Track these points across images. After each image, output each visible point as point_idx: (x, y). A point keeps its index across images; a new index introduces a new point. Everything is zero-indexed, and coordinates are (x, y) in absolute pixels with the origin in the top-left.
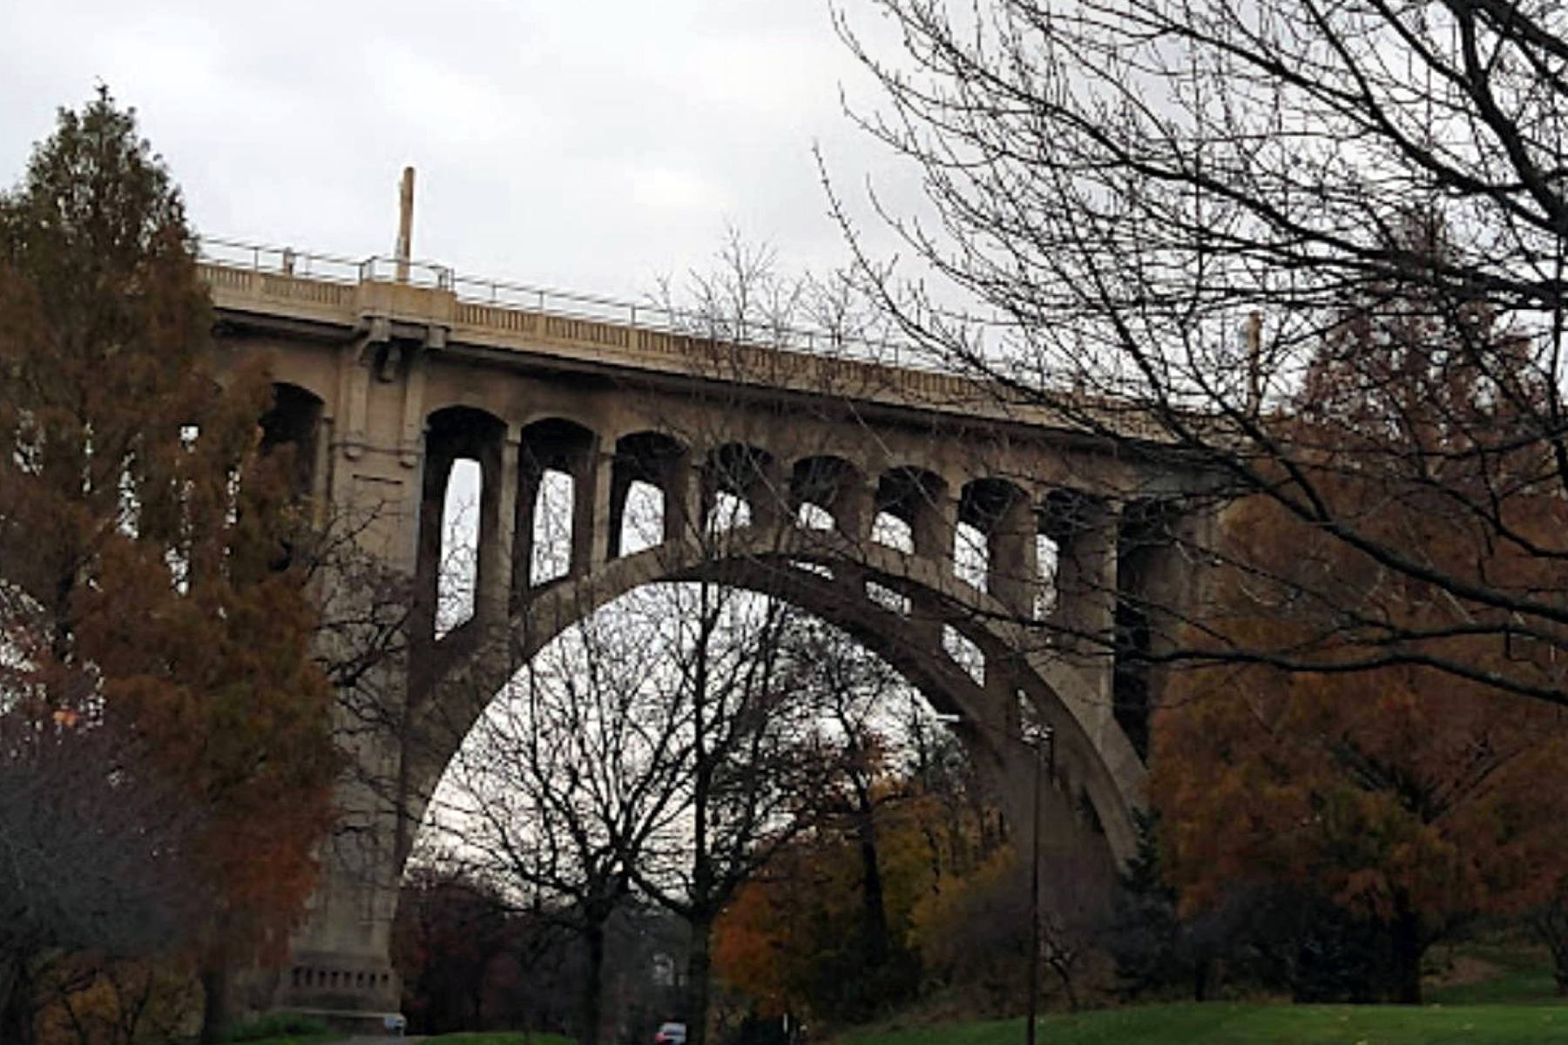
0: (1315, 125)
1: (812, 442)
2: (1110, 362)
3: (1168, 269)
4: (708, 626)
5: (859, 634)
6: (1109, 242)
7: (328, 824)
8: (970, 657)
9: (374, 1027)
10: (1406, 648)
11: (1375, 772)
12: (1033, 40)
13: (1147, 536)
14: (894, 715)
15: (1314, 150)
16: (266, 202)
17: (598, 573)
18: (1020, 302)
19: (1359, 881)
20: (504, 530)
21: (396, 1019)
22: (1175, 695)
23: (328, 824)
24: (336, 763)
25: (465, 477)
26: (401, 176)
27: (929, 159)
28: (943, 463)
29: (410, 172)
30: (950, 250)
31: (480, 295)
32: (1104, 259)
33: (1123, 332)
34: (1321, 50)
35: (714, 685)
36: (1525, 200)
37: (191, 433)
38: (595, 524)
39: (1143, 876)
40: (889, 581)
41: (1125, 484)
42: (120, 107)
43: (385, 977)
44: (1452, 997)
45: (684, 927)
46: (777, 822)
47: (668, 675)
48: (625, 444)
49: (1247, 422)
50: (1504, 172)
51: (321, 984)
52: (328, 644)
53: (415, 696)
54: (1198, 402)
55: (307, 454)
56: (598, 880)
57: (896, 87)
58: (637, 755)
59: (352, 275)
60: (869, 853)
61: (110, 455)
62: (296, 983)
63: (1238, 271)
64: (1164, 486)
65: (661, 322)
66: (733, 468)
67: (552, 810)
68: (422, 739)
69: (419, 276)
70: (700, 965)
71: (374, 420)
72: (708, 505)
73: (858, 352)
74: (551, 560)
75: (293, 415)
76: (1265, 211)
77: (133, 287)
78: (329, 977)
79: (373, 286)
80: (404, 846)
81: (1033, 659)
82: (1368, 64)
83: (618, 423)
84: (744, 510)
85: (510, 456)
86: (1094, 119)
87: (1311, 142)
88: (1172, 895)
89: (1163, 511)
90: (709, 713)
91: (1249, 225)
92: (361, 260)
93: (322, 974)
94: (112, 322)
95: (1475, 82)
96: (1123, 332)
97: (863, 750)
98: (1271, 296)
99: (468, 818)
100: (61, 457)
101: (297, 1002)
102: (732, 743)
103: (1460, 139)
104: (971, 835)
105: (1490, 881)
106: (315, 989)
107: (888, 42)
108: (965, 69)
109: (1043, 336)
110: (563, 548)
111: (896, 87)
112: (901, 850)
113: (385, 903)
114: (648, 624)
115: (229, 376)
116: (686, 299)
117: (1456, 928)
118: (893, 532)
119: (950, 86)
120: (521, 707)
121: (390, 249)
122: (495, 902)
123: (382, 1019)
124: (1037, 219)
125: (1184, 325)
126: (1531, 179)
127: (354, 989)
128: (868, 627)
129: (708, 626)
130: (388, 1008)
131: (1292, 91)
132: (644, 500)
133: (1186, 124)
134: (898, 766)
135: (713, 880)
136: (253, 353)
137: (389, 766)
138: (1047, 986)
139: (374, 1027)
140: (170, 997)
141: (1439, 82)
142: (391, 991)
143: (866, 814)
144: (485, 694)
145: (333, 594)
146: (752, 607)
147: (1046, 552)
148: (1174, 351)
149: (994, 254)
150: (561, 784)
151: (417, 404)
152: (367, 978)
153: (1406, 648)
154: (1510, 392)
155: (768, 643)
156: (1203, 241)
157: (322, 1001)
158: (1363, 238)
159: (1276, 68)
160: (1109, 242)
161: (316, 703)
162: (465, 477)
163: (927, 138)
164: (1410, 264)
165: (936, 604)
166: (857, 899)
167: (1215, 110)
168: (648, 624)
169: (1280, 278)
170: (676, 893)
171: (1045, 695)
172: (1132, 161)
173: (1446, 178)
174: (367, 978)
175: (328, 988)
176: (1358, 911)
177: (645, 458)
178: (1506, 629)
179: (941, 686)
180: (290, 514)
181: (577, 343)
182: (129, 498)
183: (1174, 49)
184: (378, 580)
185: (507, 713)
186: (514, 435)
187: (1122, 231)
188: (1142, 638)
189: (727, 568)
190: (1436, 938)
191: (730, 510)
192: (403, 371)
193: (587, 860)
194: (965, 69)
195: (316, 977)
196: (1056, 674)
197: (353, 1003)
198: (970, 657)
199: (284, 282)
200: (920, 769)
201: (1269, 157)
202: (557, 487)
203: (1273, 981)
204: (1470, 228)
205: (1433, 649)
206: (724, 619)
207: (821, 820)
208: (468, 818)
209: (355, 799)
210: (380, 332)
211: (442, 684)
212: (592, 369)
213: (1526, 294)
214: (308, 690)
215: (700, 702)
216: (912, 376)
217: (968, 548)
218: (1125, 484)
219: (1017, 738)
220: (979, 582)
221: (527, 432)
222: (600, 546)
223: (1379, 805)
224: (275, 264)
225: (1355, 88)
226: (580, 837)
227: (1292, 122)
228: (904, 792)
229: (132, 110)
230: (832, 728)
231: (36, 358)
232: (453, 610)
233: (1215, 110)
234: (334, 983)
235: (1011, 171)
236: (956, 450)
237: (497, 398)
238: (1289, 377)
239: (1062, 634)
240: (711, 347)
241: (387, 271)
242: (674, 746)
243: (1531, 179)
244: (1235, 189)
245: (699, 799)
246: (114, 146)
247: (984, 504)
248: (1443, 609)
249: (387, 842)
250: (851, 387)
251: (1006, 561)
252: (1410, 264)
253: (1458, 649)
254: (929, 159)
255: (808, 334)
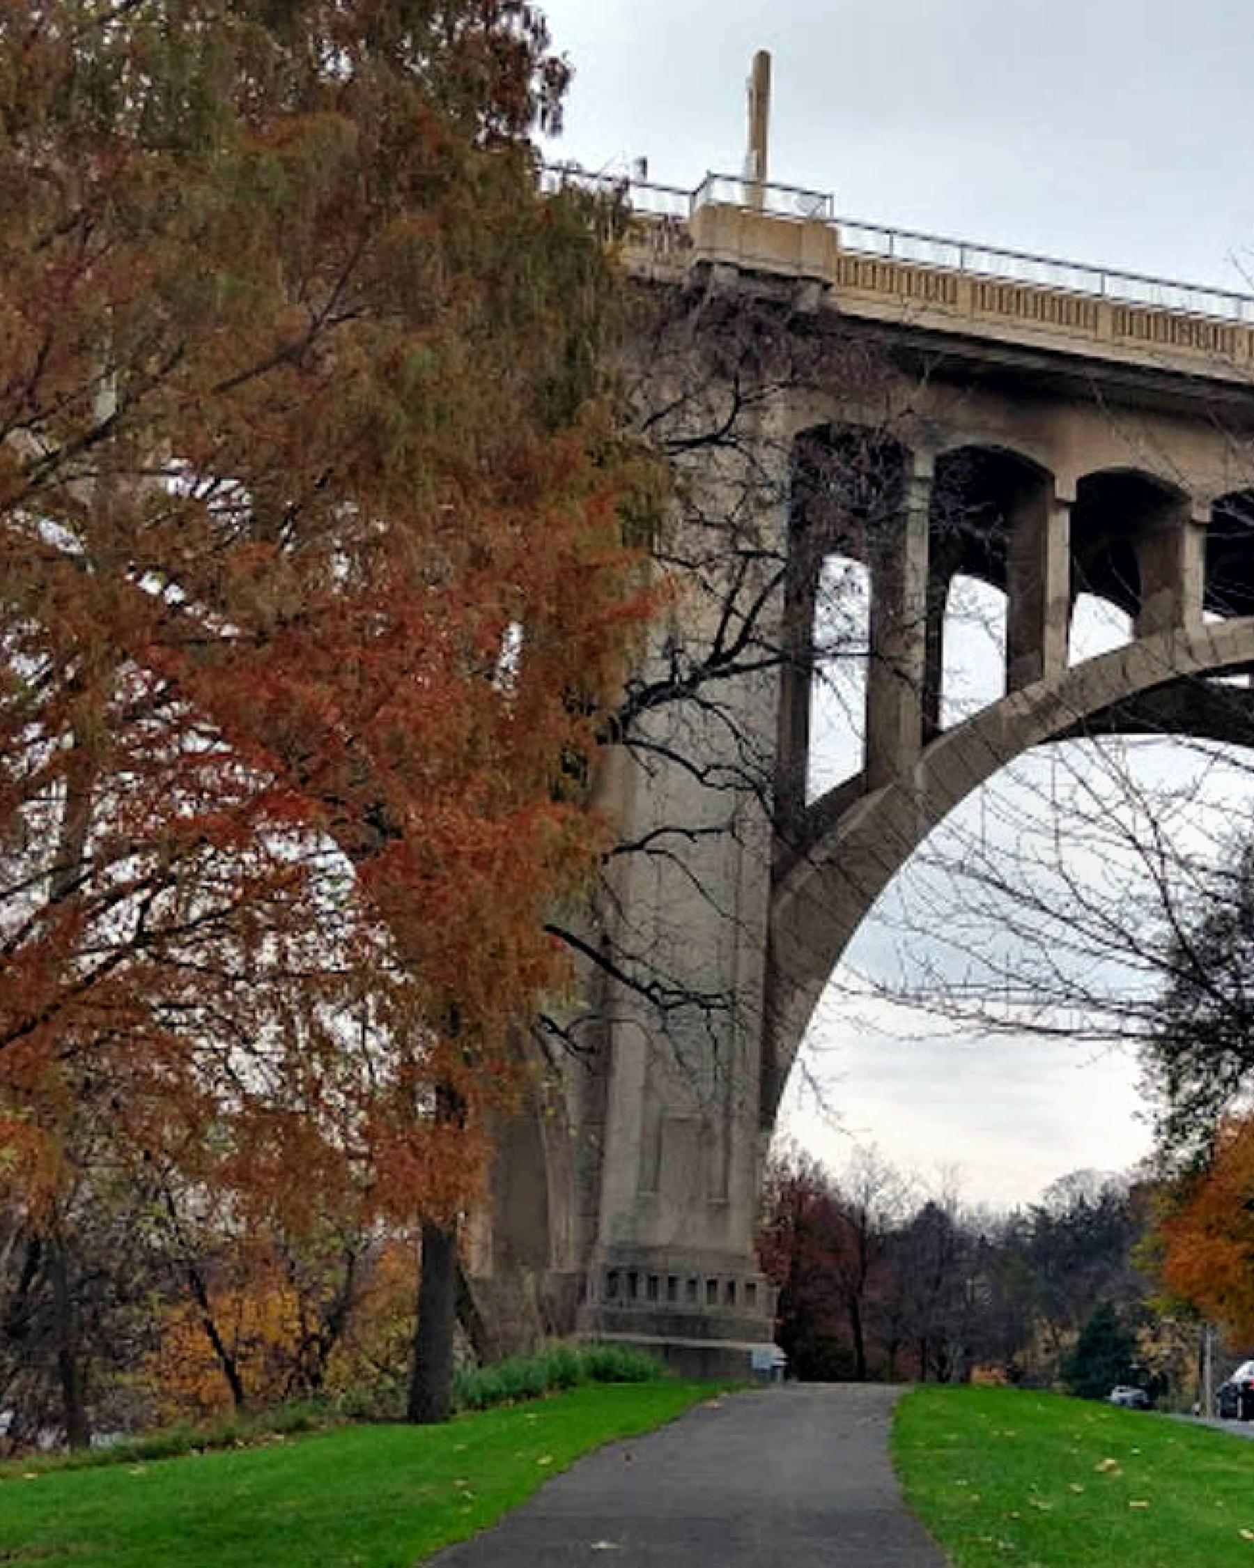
21: (770, 1354)
26: (748, 68)
29: (763, 60)
31: (872, 244)
43: (751, 1287)
51: (653, 1293)
62: (612, 1294)
78: (663, 1285)
79: (715, 213)
92: (692, 187)
93: (653, 1280)
101: (613, 1323)
106: (644, 1304)
121: (735, 160)
123: (750, 1353)
127: (702, 1305)
130: (752, 1334)
142: (761, 1310)
144: (904, 849)
152: (721, 1287)
157: (659, 1322)
161: (294, 775)
174: (721, 1287)
175: (662, 1301)
181: (1022, 321)
186: (923, 467)
195: (642, 1287)
197: (701, 1325)
212: (1039, 363)
221: (941, 464)
229: (874, 1145)
234: (672, 1296)
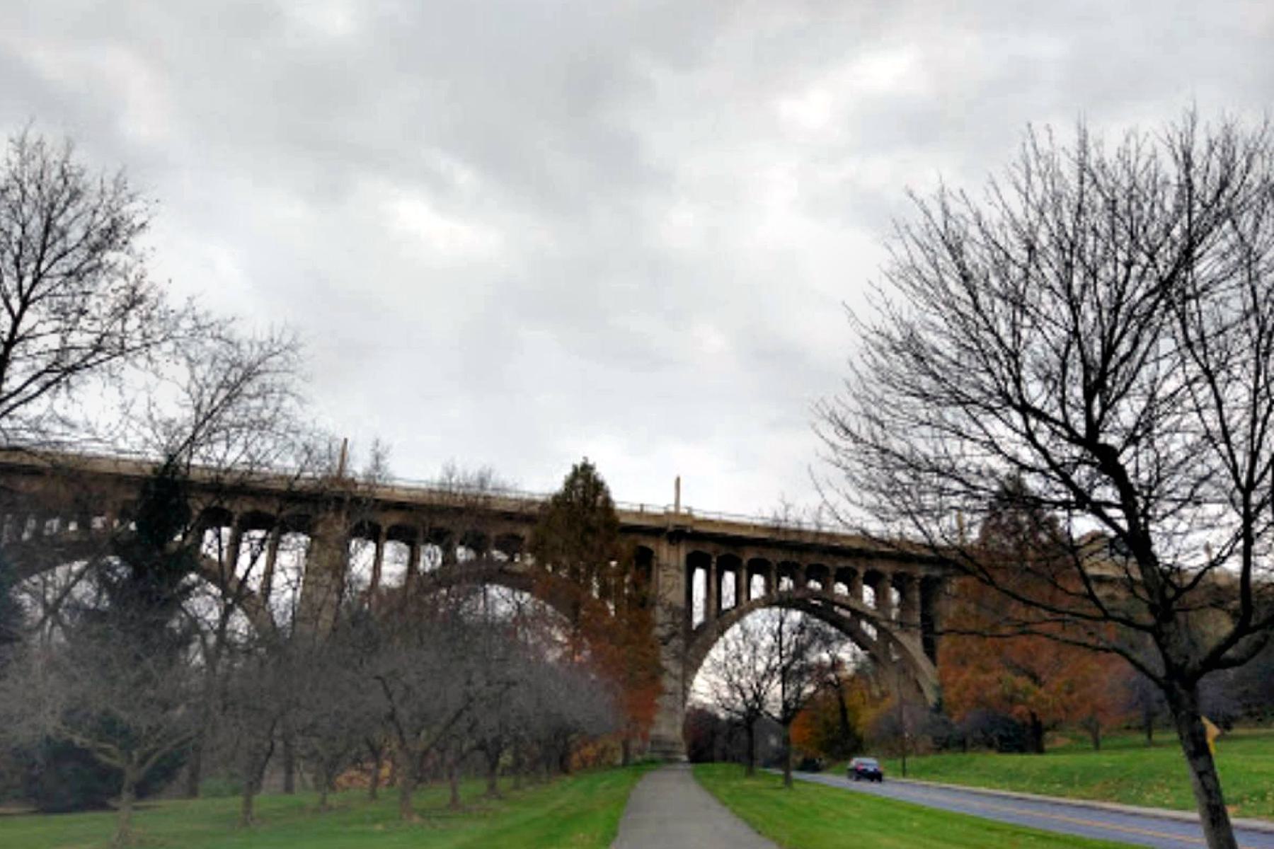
0: (975, 452)
1: (813, 559)
2: (912, 532)
3: (929, 500)
4: (782, 622)
5: (833, 623)
6: (909, 493)
7: (661, 691)
8: (871, 632)
9: (677, 761)
10: (1027, 628)
11: (1019, 670)
12: (877, 429)
13: (930, 588)
14: (847, 652)
15: (977, 460)
16: (635, 490)
17: (744, 606)
18: (875, 510)
19: (1020, 708)
20: (714, 593)
21: (685, 758)
22: (944, 644)
23: (661, 691)
24: (663, 670)
25: (700, 575)
27: (846, 468)
28: (857, 564)
29: (678, 480)
30: (855, 497)
32: (908, 499)
33: (917, 523)
34: (974, 427)
35: (785, 643)
36: (1053, 473)
37: (613, 563)
38: (742, 589)
39: (938, 708)
40: (843, 606)
41: (921, 571)
42: (590, 462)
44: (1055, 751)
45: (780, 727)
46: (809, 689)
47: (769, 639)
48: (751, 562)
49: (962, 551)
50: (1044, 464)
52: (659, 632)
53: (687, 647)
54: (944, 543)
55: (649, 569)
56: (751, 709)
57: (833, 445)
58: (761, 667)
59: (661, 511)
60: (841, 699)
61: (590, 570)
63: (955, 501)
64: (937, 573)
65: (759, 522)
66: (787, 569)
67: (733, 686)
68: (690, 663)
69: (683, 511)
70: (786, 741)
71: (670, 556)
72: (779, 581)
73: (826, 529)
74: (728, 601)
75: (644, 559)
76: (961, 481)
77: (595, 518)
79: (668, 514)
80: (685, 698)
81: (895, 634)
82: (992, 432)
83: (749, 555)
84: (791, 584)
85: (713, 567)
86: (900, 452)
87: (973, 456)
88: (951, 715)
89: (938, 581)
90: (784, 653)
91: (956, 486)
94: (590, 529)
95: (1030, 436)
96: (917, 523)
97: (837, 664)
98: (967, 509)
99: (707, 688)
100: (574, 572)
101: (653, 751)
102: (791, 663)
103: (1027, 455)
104: (877, 693)
105: (1066, 710)
107: (830, 433)
108: (856, 440)
109: (889, 525)
110: (732, 598)
111: (833, 445)
112: (853, 699)
113: (680, 719)
114: (761, 621)
115: (625, 545)
116: (768, 514)
117: (1054, 726)
118: (841, 588)
119: (850, 445)
120: (722, 652)
121: (673, 502)
122: (715, 718)
124: (884, 487)
125: (938, 519)
126: (1053, 466)
128: (837, 622)
129: (782, 622)
131: (967, 443)
132: (758, 581)
133: (931, 453)
134: (849, 669)
135: (790, 711)
136: (632, 537)
137: (679, 671)
138: (908, 747)
139: (677, 761)
140: (613, 750)
141: (1018, 437)
142: (683, 748)
143: (839, 686)
145: (660, 615)
146: (796, 616)
147: (895, 596)
148: (935, 528)
149: (870, 498)
150: (736, 678)
151: (683, 552)
153: (1027, 628)
154: (1053, 536)
155: (802, 628)
156: (941, 491)
158: (995, 488)
159: (960, 434)
160: (909, 493)
162: (700, 575)
163: (844, 461)
164: (1013, 495)
165: (858, 614)
166: (838, 716)
167: (942, 450)
168: (761, 621)
169: (969, 503)
170: (776, 715)
171: (900, 647)
172: (913, 465)
173: (1023, 467)
176: (1018, 721)
177: (758, 567)
178: (1063, 621)
179: (861, 641)
180: (645, 589)
182: (596, 585)
183: (925, 430)
184: (672, 608)
185: (717, 653)
186: (714, 560)
187: (914, 491)
188: (932, 626)
189: (787, 602)
190: (1048, 729)
191: (786, 583)
192: (679, 541)
193: (745, 703)
194: (856, 440)
196: (904, 639)
198: (871, 632)
199: (640, 514)
200: (857, 671)
201: (961, 463)
202: (729, 577)
203: (990, 745)
204: (1033, 483)
205: (1036, 628)
206: (787, 620)
207: (825, 687)
208: (707, 688)
209: (669, 683)
210: (671, 529)
211: (696, 643)
213: (1056, 504)
214: (652, 647)
215: (781, 649)
216: (846, 537)
217: (868, 593)
218: (921, 571)
219: (890, 659)
220: (871, 605)
221: (719, 559)
222: (744, 597)
223: (1023, 682)
224: (637, 508)
225: (987, 439)
226: (743, 695)
227: (968, 451)
228: (852, 679)
230: (825, 657)
231: (566, 541)
232: (698, 618)
233: (942, 450)
235: (874, 471)
236: (862, 561)
237: (708, 548)
238: (975, 534)
239: (903, 625)
240: (777, 529)
241: (672, 509)
242: (773, 664)
243: (1053, 466)
244: (951, 473)
245: (783, 681)
246: (589, 475)
247: (873, 579)
248: (1038, 615)
249: (680, 697)
250: (822, 540)
251: (880, 596)
252: (1013, 495)
253: (1045, 627)
254: (846, 468)
255: (809, 524)
